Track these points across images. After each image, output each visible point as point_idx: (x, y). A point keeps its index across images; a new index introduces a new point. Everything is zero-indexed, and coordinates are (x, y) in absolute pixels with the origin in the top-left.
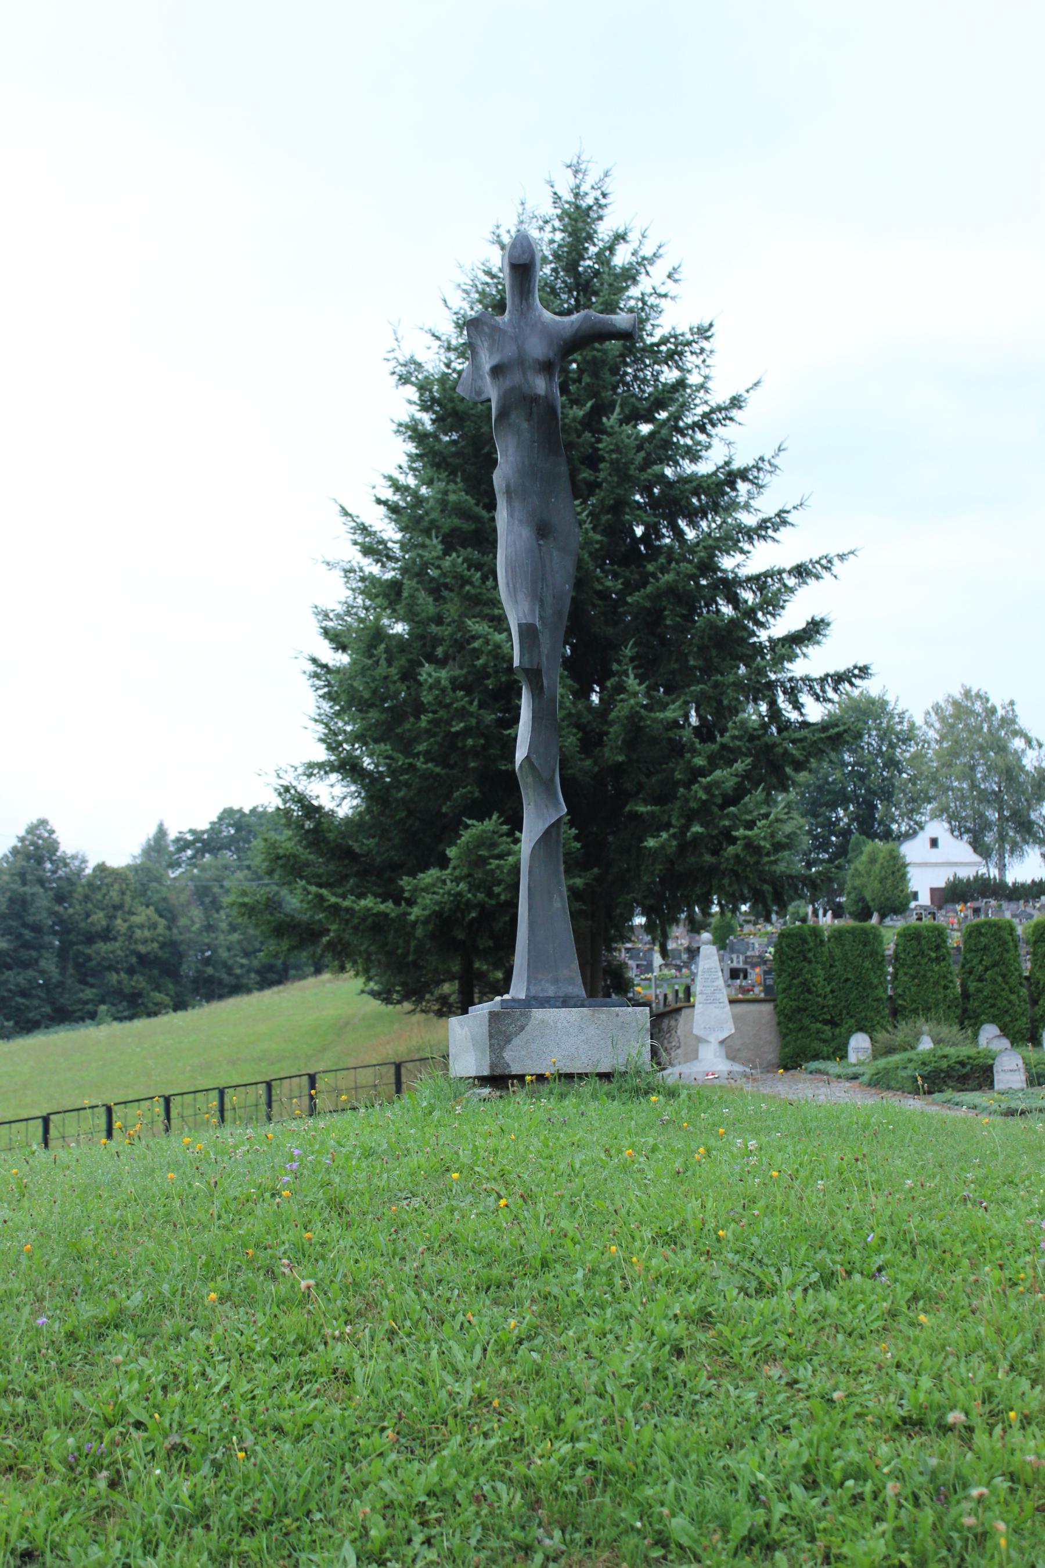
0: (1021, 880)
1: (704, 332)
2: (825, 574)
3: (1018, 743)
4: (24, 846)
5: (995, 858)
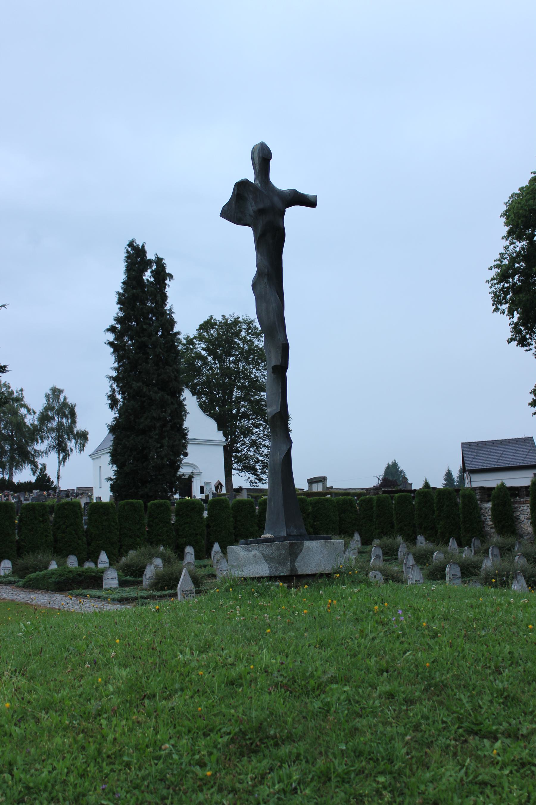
0: (22, 481)
3: (23, 411)
5: (7, 470)
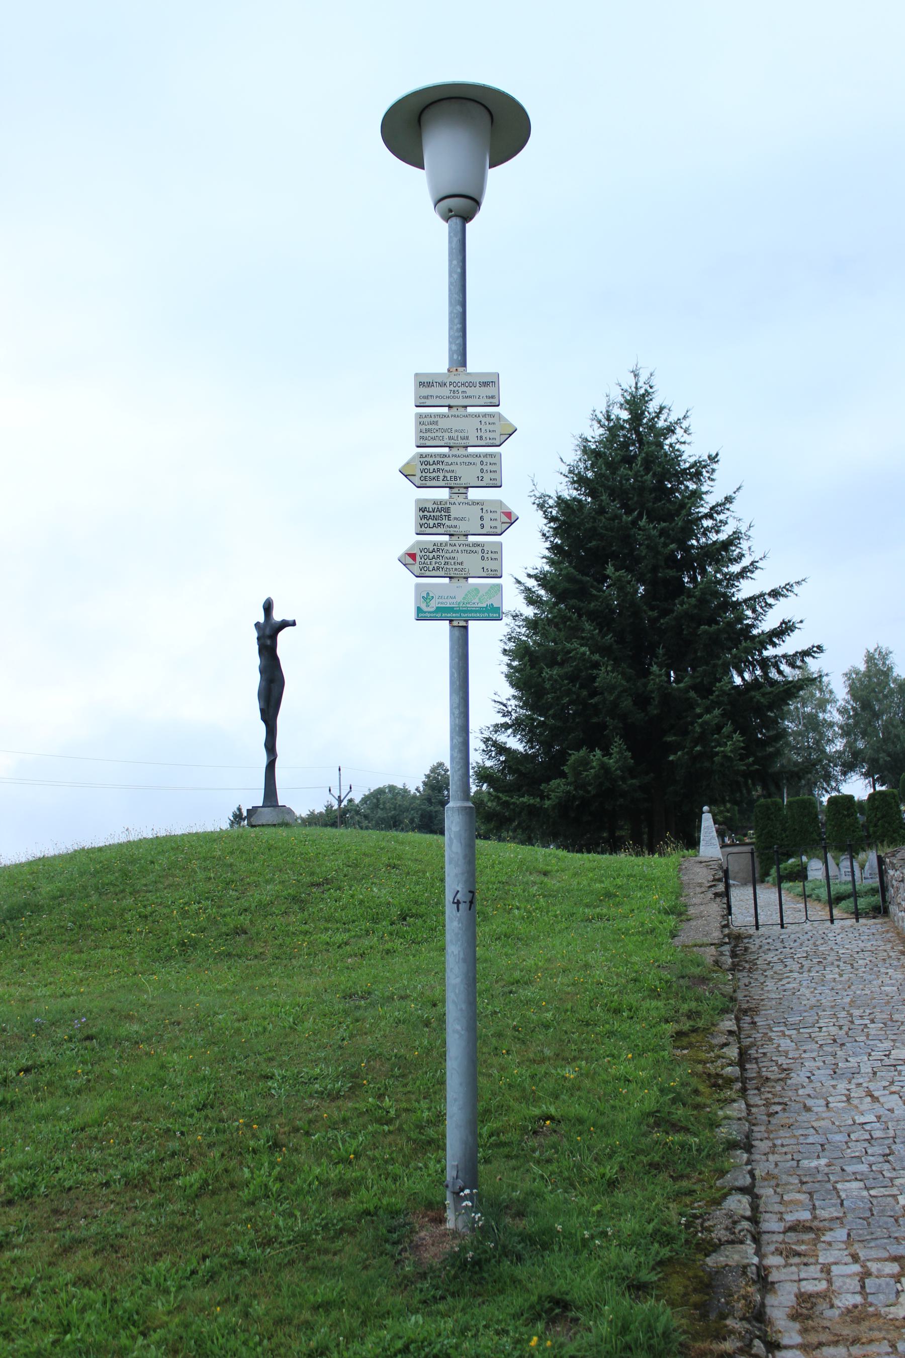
1: (713, 459)
2: (789, 594)
4: (430, 781)
